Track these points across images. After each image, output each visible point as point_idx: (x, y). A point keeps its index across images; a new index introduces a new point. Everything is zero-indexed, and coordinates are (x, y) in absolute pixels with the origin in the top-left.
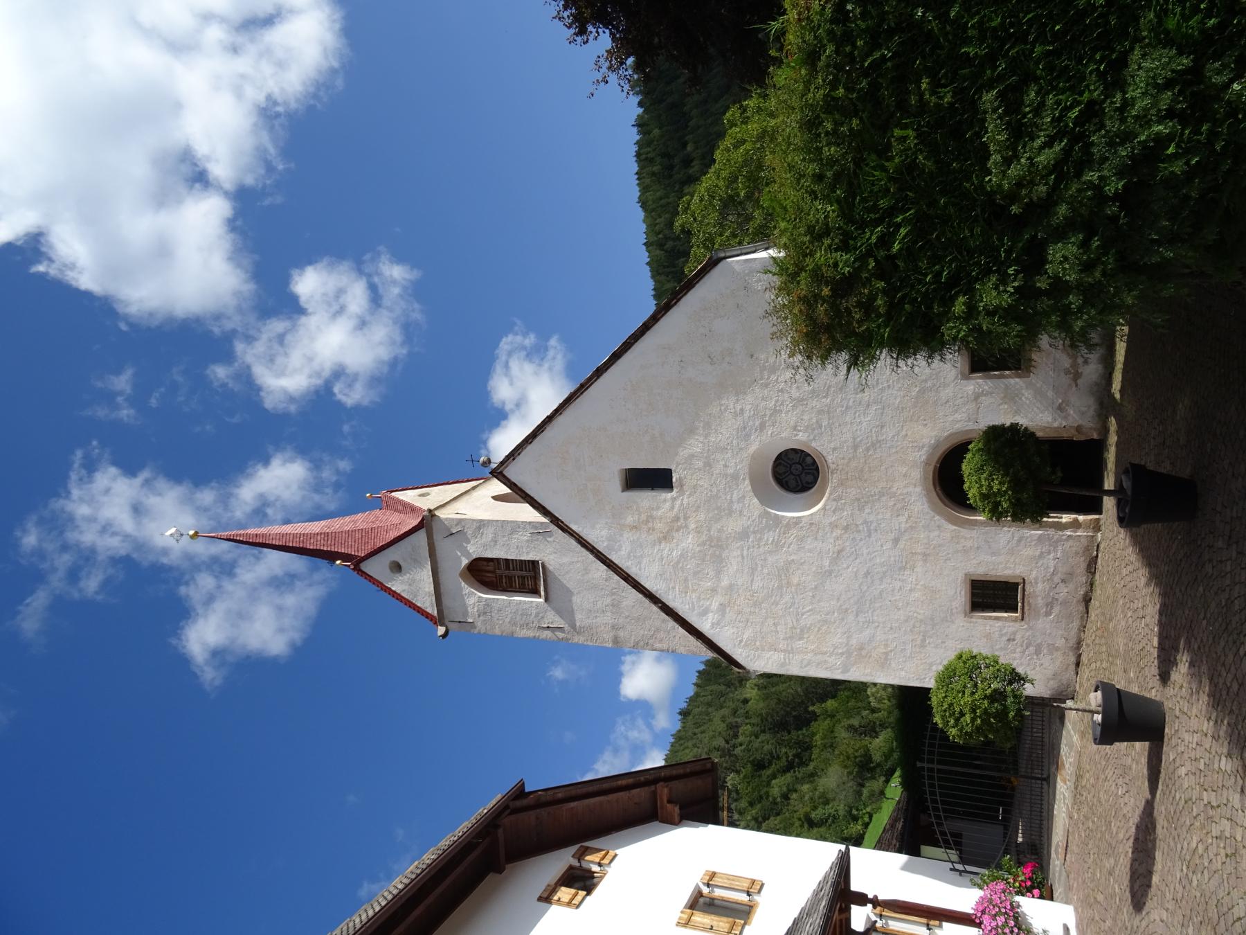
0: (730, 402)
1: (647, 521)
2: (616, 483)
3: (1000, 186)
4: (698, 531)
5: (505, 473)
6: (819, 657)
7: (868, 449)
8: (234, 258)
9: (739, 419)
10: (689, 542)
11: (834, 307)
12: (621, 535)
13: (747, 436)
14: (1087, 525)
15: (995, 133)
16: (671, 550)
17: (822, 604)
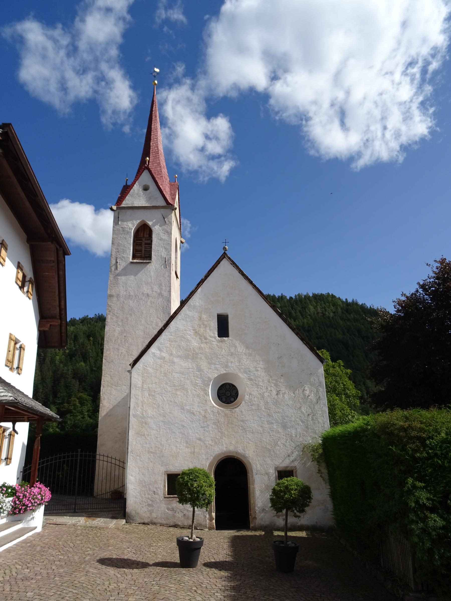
0: (261, 365)
1: (204, 325)
2: (221, 312)
4: (200, 348)
5: (225, 259)
7: (242, 426)
8: (235, 87)
9: (254, 369)
10: (195, 343)
12: (196, 312)
14: (211, 524)
16: (190, 335)
17: (167, 405)
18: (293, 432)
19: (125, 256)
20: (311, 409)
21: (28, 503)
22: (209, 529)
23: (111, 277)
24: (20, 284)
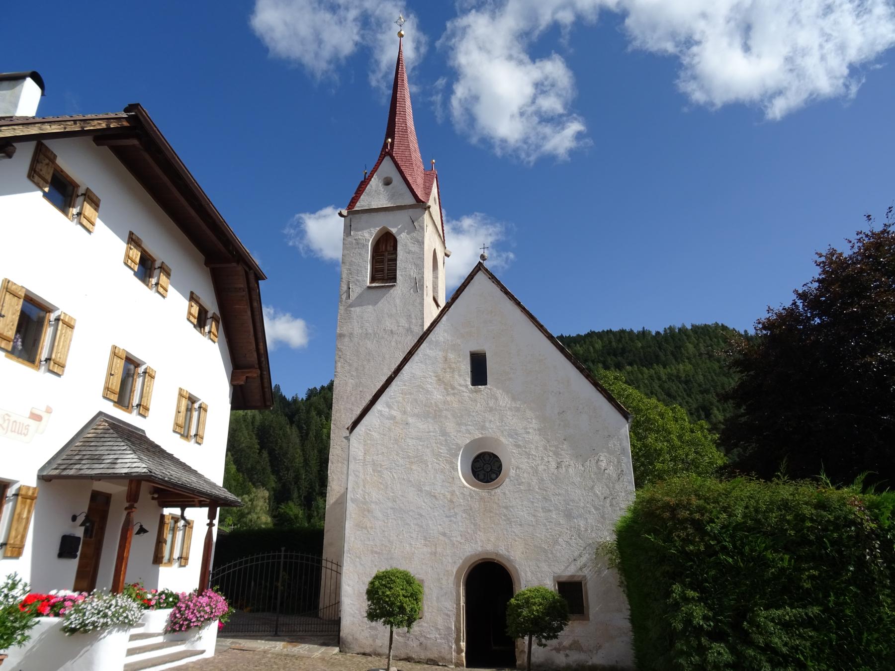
0: (535, 424)
1: (450, 368)
2: (476, 348)
3: (758, 615)
6: (362, 483)
7: (505, 516)
10: (438, 396)
11: (686, 520)
13: (512, 437)
14: (459, 658)
15: (788, 613)
17: (399, 485)
18: (582, 523)
19: (360, 278)
20: (609, 488)
21: (191, 616)
22: (456, 666)
23: (342, 309)
24: (195, 321)
